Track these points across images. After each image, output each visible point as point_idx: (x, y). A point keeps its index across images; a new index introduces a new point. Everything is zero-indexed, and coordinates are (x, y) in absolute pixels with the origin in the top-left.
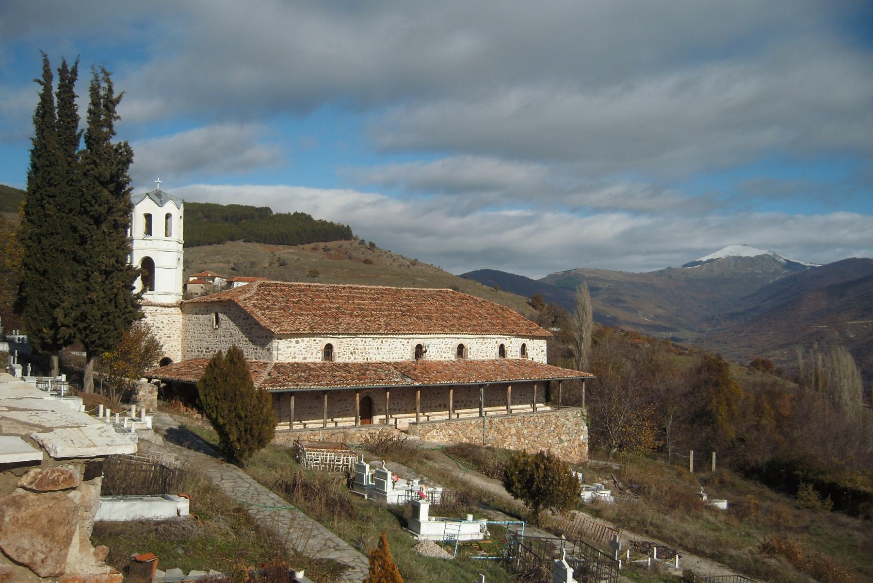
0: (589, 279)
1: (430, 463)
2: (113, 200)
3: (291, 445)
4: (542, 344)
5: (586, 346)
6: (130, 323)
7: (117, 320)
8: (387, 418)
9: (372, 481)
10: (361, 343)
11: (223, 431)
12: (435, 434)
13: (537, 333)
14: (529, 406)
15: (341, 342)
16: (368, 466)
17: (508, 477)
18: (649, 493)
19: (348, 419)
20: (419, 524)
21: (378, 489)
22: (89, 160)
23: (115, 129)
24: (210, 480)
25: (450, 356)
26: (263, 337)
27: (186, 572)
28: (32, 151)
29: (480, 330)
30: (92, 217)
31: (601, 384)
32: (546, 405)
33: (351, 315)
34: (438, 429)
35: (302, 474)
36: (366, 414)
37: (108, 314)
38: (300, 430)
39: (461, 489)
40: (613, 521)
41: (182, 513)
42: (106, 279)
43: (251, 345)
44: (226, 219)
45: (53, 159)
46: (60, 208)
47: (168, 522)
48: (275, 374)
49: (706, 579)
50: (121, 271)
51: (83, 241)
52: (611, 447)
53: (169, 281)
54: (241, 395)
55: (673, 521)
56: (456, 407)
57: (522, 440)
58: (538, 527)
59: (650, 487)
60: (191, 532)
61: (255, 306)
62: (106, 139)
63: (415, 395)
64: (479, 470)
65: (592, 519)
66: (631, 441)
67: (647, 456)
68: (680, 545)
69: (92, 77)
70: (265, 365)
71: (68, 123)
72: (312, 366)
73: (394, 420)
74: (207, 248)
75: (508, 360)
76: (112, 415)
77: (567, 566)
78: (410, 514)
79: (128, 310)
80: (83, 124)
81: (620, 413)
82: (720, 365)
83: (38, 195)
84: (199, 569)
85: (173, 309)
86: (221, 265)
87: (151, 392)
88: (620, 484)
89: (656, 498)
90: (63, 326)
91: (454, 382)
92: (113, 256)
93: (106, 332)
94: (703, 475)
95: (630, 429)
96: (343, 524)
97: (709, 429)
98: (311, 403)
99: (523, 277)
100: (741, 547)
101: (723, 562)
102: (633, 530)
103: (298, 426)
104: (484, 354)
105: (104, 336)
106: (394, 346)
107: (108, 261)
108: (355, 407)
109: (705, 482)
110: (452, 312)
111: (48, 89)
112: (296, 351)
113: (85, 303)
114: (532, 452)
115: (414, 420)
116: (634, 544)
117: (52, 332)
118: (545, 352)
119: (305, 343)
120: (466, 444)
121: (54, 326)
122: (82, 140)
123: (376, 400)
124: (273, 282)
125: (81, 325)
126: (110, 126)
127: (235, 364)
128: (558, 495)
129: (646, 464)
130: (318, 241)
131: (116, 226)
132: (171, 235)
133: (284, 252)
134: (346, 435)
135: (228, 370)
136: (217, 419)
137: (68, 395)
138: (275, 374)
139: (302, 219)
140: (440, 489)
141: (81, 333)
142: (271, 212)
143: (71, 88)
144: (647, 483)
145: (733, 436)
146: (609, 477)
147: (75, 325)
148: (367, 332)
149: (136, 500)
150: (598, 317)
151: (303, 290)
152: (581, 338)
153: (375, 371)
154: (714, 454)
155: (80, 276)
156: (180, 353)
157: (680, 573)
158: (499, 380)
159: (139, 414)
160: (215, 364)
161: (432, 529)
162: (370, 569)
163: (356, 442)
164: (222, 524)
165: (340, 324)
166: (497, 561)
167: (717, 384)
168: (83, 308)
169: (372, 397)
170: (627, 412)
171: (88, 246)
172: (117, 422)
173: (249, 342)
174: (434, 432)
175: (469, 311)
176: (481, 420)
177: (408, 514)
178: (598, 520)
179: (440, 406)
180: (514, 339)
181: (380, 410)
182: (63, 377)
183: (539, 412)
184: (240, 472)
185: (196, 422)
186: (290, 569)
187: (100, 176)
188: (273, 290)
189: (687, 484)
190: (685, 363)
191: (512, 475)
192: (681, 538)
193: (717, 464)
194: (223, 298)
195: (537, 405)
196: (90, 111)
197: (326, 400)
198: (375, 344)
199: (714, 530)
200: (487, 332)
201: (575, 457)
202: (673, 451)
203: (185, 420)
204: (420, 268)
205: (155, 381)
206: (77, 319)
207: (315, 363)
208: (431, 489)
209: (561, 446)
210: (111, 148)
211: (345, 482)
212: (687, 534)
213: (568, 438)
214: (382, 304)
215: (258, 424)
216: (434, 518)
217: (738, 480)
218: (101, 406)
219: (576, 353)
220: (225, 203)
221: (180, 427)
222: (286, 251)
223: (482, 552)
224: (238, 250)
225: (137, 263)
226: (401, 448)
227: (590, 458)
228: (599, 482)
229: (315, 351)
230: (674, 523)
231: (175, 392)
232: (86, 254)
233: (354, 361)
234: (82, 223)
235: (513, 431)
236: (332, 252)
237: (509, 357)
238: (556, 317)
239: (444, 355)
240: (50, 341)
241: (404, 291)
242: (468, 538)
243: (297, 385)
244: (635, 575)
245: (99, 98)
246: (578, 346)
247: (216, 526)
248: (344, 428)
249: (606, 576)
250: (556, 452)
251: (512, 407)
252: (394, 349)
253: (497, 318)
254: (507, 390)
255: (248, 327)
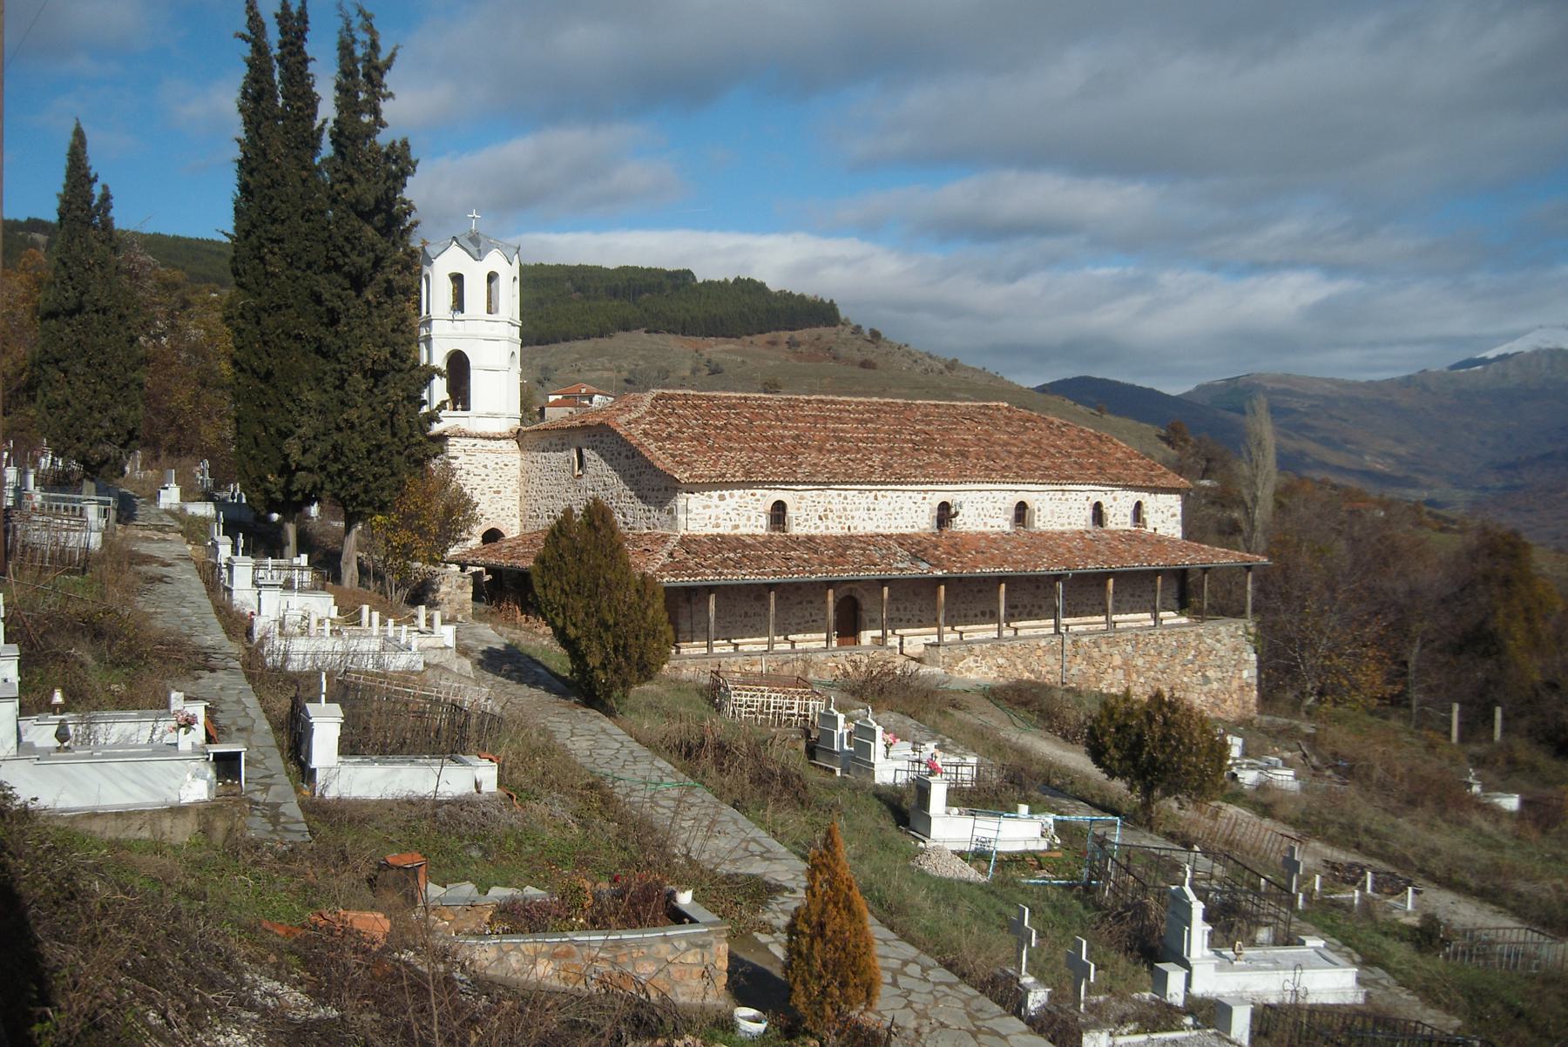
0: (1273, 392)
1: (958, 714)
2: (382, 244)
3: (706, 680)
4: (1174, 502)
5: (1263, 512)
6: (420, 463)
7: (396, 458)
8: (884, 637)
9: (849, 744)
10: (837, 499)
11: (577, 650)
12: (972, 664)
13: (1163, 483)
14: (1148, 615)
15: (802, 498)
16: (841, 717)
17: (1096, 739)
18: (1368, 776)
19: (814, 636)
20: (928, 820)
21: (860, 758)
22: (339, 176)
23: (384, 117)
24: (551, 735)
25: (1003, 523)
26: (658, 488)
27: (483, 888)
28: (239, 162)
29: (1057, 475)
30: (348, 275)
31: (1287, 579)
32: (1181, 614)
33: (820, 450)
34: (976, 655)
35: (716, 726)
36: (848, 626)
37: (379, 447)
38: (728, 655)
39: (1012, 759)
40: (1295, 823)
41: (484, 788)
42: (375, 386)
43: (639, 504)
44: (614, 293)
45: (277, 175)
46: (292, 260)
47: (459, 803)
48: (680, 555)
49: (1465, 932)
50: (401, 370)
51: (333, 319)
52: (1303, 694)
53: (497, 390)
54: (607, 586)
55: (1409, 828)
56: (1010, 617)
57: (1134, 677)
58: (1151, 830)
59: (1371, 767)
60: (495, 820)
61: (646, 434)
62: (368, 136)
63: (936, 593)
64: (1049, 728)
65: (1256, 819)
66: (1340, 685)
67: (1372, 714)
68: (1421, 871)
69: (340, 24)
70: (664, 539)
71: (300, 109)
72: (749, 541)
73: (898, 640)
74: (580, 345)
75: (1109, 532)
76: (383, 622)
77: (1192, 897)
78: (914, 803)
79: (413, 440)
80: (327, 111)
81: (1321, 632)
82: (1513, 546)
83: (253, 238)
84: (507, 884)
85: (503, 442)
86: (606, 374)
87: (460, 587)
88: (1314, 760)
89: (1382, 786)
90: (300, 468)
91: (1008, 569)
92: (384, 345)
93: (376, 479)
94: (1475, 749)
95: (1336, 661)
96: (795, 821)
97: (1489, 664)
98: (746, 606)
99: (1151, 391)
100: (1540, 878)
101: (1502, 905)
102: (1331, 841)
103: (722, 648)
104: (1065, 521)
105: (373, 486)
106: (899, 505)
107: (376, 354)
108: (826, 614)
109: (1479, 762)
110: (1006, 444)
111: (260, 49)
112: (719, 513)
113: (339, 429)
114: (1141, 692)
115: (935, 639)
116: (1333, 866)
117: (282, 481)
118: (1179, 518)
119: (736, 499)
120: (1029, 681)
121: (286, 471)
122: (326, 139)
123: (866, 603)
124: (680, 392)
125: (334, 468)
126: (376, 112)
127: (597, 530)
128: (1188, 773)
129: (1369, 726)
130: (777, 329)
131: (389, 291)
132: (497, 311)
133: (718, 349)
134: (807, 663)
135: (581, 544)
136: (564, 628)
137: (313, 589)
138: (680, 555)
139: (749, 289)
140: (972, 760)
141: (332, 481)
142: (694, 278)
143: (301, 47)
144: (1366, 759)
145: (1537, 677)
146: (1294, 745)
147: (322, 468)
148: (849, 479)
149: (403, 763)
150: (1286, 462)
151: (734, 407)
152: (1255, 499)
153: (864, 549)
154: (1498, 712)
155: (330, 379)
156: (517, 521)
157: (1414, 921)
158: (1091, 566)
159: (430, 621)
160: (560, 530)
161: (950, 830)
162: (807, 889)
163: (828, 678)
164: (557, 809)
165: (800, 465)
166: (1069, 887)
167: (1507, 582)
168: (337, 436)
169: (858, 596)
170: (1333, 629)
171: (341, 328)
172: (391, 634)
173: (635, 499)
174: (970, 661)
175: (1038, 443)
176: (1057, 640)
177: (910, 802)
178: (1267, 822)
179: (983, 614)
180: (1119, 493)
181: (873, 621)
182: (303, 559)
183: (1166, 627)
184: (607, 723)
185: (538, 639)
186: (669, 887)
187: (358, 201)
188: (680, 407)
189: (1446, 762)
190: (1447, 544)
191: (1103, 735)
192: (1423, 859)
193: (1504, 730)
194: (589, 421)
195: (1162, 614)
196: (339, 87)
197: (772, 600)
198: (863, 501)
199: (1490, 847)
200: (1071, 479)
201: (1232, 709)
202: (1421, 704)
203: (518, 635)
204: (962, 374)
205: (474, 569)
206: (326, 457)
207: (753, 536)
208: (955, 760)
209: (1206, 689)
210: (378, 152)
211: (802, 745)
212: (1435, 852)
213: (1220, 675)
214: (877, 430)
215: (637, 638)
216: (955, 810)
217: (1542, 759)
218: (366, 608)
219: (1244, 526)
220: (611, 263)
221: (507, 646)
222: (721, 347)
223: (1043, 873)
224: (636, 346)
225: (439, 361)
226: (907, 686)
227: (1260, 713)
228: (1274, 754)
229: (754, 514)
230: (1410, 831)
231: (501, 588)
232: (340, 343)
233: (825, 532)
234: (328, 286)
235: (1117, 660)
236: (803, 348)
237: (1111, 525)
238: (1208, 461)
239: (991, 522)
240: (279, 496)
241: (918, 407)
242: (1019, 847)
243: (721, 574)
244: (1328, 922)
245: (354, 61)
246: (1248, 513)
247: (546, 811)
248: (805, 651)
249: (1270, 920)
250: (1197, 699)
251: (1115, 618)
252: (901, 511)
253: (1090, 455)
254: (1106, 585)
255: (634, 472)
